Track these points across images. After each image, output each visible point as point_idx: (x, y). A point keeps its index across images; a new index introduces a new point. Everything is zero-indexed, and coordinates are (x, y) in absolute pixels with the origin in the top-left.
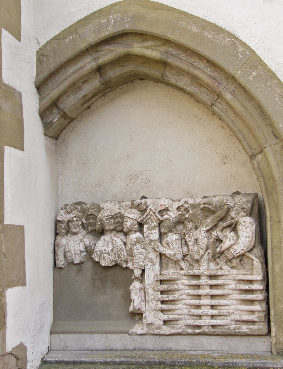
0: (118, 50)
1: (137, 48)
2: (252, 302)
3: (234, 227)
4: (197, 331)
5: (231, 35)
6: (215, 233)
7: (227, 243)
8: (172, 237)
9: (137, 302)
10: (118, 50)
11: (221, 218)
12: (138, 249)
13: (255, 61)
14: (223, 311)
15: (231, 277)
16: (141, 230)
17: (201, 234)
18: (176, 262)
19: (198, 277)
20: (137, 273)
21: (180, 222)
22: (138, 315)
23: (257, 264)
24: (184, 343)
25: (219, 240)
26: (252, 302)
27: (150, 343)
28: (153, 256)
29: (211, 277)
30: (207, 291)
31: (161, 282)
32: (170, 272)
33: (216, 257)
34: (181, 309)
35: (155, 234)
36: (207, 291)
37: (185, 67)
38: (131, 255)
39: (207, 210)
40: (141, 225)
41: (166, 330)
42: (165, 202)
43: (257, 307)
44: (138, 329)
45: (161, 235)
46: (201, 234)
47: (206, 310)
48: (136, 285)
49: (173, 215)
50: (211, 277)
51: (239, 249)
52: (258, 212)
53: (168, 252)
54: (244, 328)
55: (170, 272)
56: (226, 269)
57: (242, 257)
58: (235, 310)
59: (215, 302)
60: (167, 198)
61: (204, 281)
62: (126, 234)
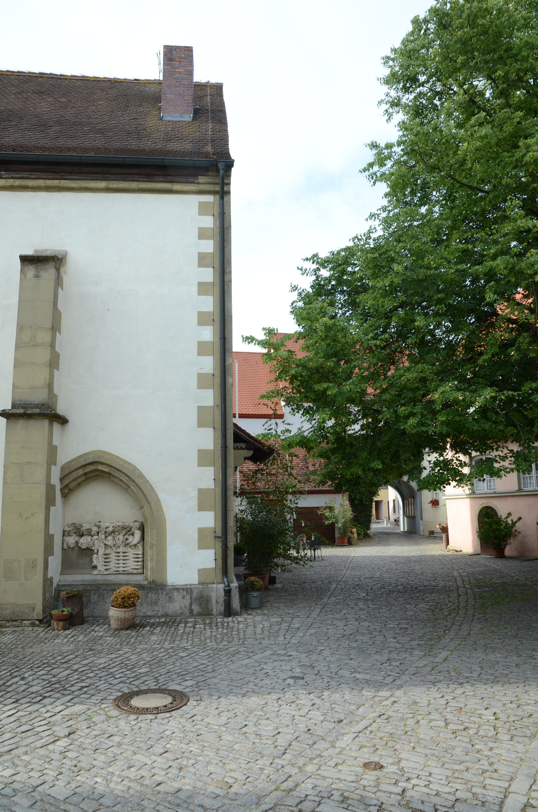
0: (93, 467)
1: (100, 467)
2: (138, 562)
3: (133, 534)
4: (118, 573)
5: (134, 466)
6: (126, 537)
7: (130, 540)
8: (110, 538)
9: (95, 562)
10: (93, 467)
11: (129, 531)
12: (96, 542)
13: (142, 476)
14: (127, 565)
15: (131, 553)
16: (98, 535)
17: (121, 537)
18: (111, 547)
19: (119, 553)
20: (96, 551)
21: (113, 532)
22: (95, 567)
23: (141, 548)
24: (113, 578)
25: (127, 539)
26: (138, 562)
27: (99, 578)
28: (102, 545)
29: (124, 553)
30: (122, 558)
31: (105, 555)
32: (108, 551)
33: (126, 545)
34: (112, 565)
35: (103, 537)
36: (122, 558)
37: (118, 476)
38: (94, 544)
39: (124, 528)
40: (98, 533)
41: (106, 573)
42: (108, 524)
43: (140, 563)
44: (95, 572)
45: (106, 537)
46: (121, 537)
47: (121, 565)
48: (95, 556)
49: (110, 529)
50: (124, 553)
51: (134, 542)
52: (142, 528)
53: (108, 543)
54: (135, 571)
55: (108, 551)
56: (129, 550)
57: (135, 545)
58: (132, 565)
59: (124, 562)
60: (108, 523)
61: (121, 554)
62: (92, 536)
